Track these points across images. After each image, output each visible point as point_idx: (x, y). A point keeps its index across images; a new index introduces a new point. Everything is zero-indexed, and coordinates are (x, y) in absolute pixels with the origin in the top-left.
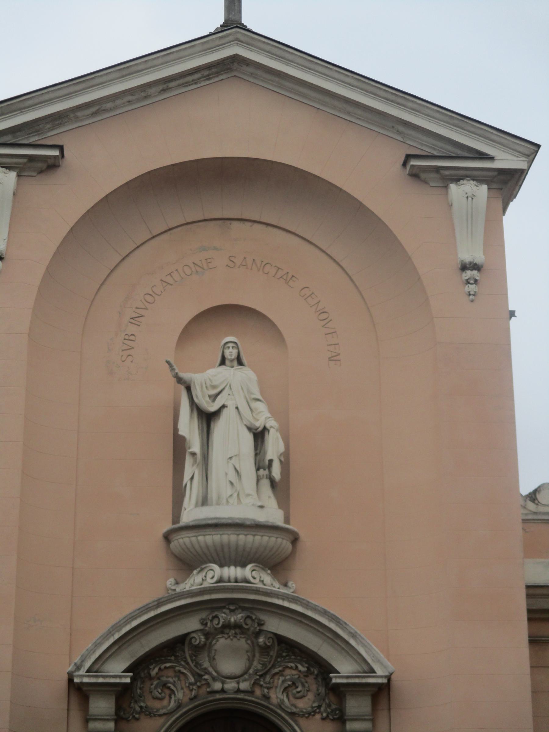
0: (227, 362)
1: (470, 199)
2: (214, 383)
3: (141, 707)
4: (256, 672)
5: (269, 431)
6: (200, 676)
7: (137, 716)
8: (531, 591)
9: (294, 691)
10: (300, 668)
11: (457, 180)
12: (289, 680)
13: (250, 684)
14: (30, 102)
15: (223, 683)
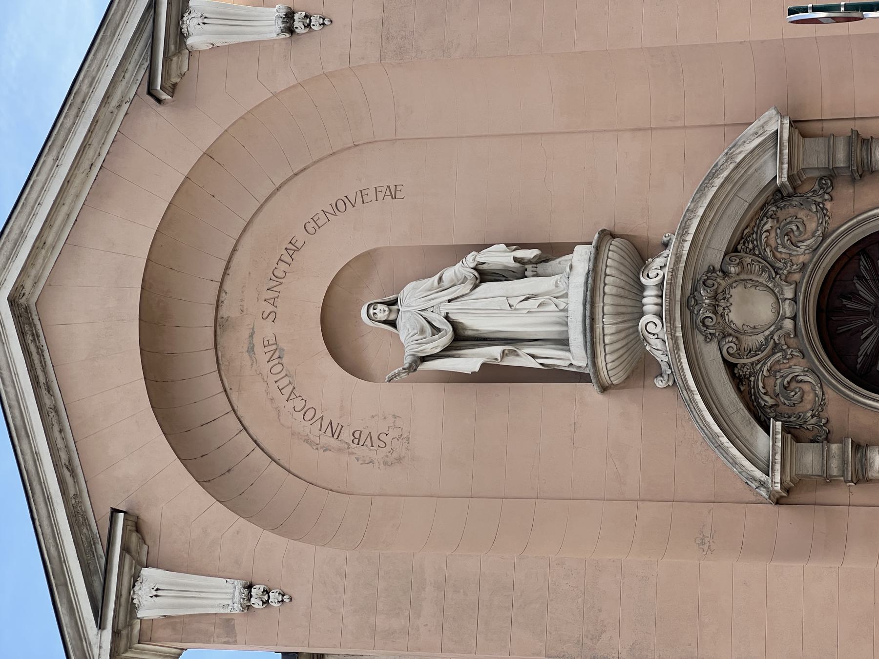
0: (392, 317)
1: (206, 21)
3: (813, 416)
7: (824, 421)
9: (796, 233)
10: (767, 227)
13: (786, 286)
14: (53, 550)
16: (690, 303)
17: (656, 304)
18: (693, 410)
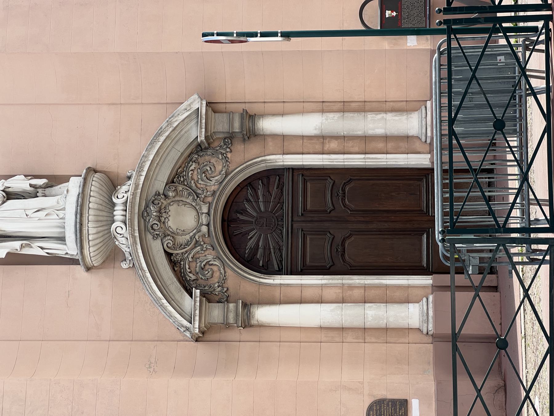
3: (218, 286)
7: (225, 289)
9: (210, 172)
10: (192, 168)
12: (201, 176)
13: (203, 205)
16: (144, 214)
17: (123, 215)
18: (145, 282)
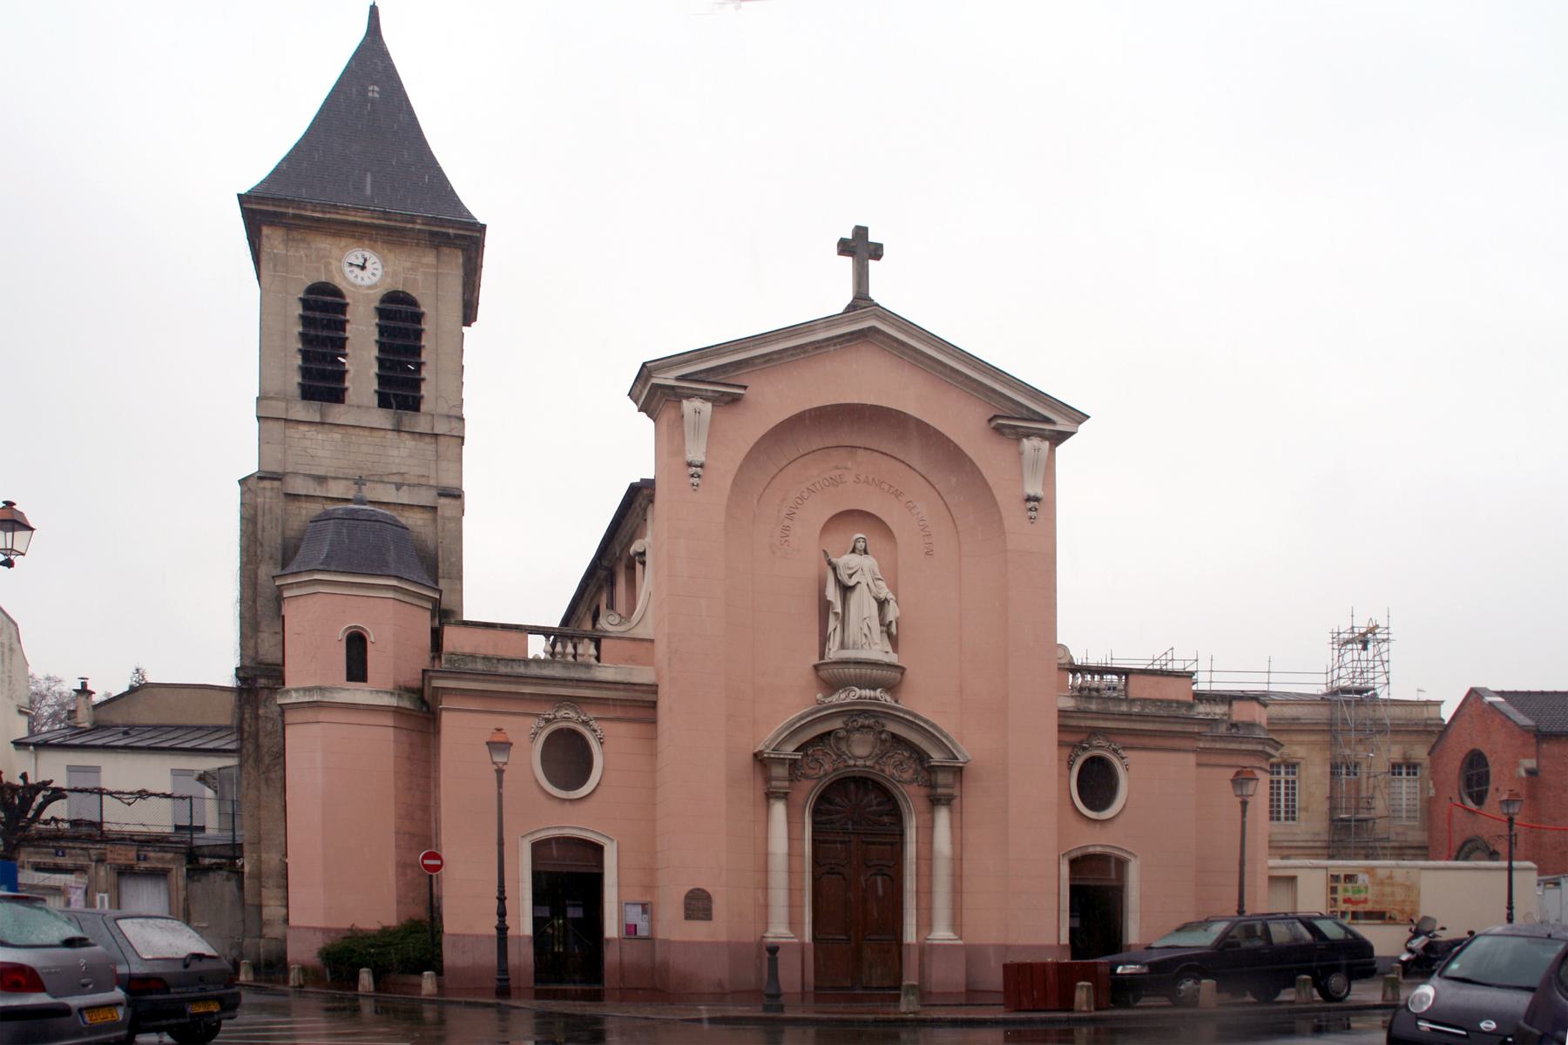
0: (857, 551)
2: (850, 566)
4: (877, 755)
5: (889, 602)
6: (841, 756)
8: (1062, 714)
10: (905, 754)
11: (1028, 436)
15: (855, 761)
